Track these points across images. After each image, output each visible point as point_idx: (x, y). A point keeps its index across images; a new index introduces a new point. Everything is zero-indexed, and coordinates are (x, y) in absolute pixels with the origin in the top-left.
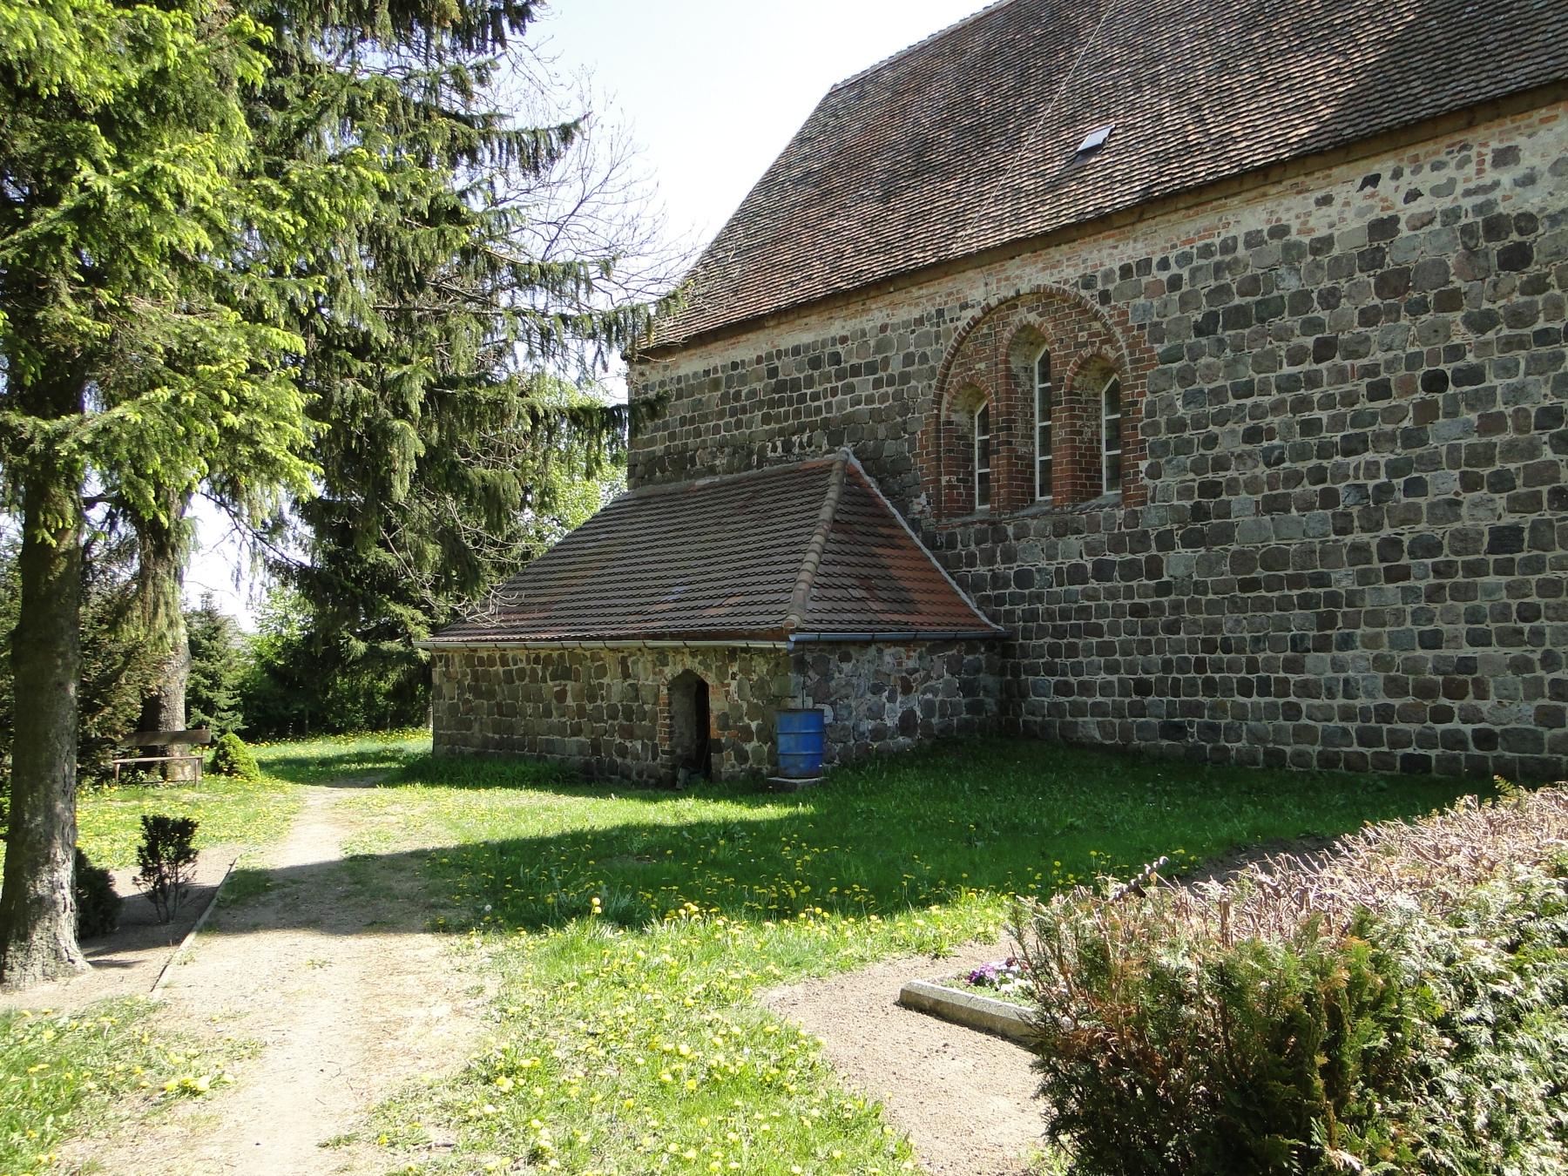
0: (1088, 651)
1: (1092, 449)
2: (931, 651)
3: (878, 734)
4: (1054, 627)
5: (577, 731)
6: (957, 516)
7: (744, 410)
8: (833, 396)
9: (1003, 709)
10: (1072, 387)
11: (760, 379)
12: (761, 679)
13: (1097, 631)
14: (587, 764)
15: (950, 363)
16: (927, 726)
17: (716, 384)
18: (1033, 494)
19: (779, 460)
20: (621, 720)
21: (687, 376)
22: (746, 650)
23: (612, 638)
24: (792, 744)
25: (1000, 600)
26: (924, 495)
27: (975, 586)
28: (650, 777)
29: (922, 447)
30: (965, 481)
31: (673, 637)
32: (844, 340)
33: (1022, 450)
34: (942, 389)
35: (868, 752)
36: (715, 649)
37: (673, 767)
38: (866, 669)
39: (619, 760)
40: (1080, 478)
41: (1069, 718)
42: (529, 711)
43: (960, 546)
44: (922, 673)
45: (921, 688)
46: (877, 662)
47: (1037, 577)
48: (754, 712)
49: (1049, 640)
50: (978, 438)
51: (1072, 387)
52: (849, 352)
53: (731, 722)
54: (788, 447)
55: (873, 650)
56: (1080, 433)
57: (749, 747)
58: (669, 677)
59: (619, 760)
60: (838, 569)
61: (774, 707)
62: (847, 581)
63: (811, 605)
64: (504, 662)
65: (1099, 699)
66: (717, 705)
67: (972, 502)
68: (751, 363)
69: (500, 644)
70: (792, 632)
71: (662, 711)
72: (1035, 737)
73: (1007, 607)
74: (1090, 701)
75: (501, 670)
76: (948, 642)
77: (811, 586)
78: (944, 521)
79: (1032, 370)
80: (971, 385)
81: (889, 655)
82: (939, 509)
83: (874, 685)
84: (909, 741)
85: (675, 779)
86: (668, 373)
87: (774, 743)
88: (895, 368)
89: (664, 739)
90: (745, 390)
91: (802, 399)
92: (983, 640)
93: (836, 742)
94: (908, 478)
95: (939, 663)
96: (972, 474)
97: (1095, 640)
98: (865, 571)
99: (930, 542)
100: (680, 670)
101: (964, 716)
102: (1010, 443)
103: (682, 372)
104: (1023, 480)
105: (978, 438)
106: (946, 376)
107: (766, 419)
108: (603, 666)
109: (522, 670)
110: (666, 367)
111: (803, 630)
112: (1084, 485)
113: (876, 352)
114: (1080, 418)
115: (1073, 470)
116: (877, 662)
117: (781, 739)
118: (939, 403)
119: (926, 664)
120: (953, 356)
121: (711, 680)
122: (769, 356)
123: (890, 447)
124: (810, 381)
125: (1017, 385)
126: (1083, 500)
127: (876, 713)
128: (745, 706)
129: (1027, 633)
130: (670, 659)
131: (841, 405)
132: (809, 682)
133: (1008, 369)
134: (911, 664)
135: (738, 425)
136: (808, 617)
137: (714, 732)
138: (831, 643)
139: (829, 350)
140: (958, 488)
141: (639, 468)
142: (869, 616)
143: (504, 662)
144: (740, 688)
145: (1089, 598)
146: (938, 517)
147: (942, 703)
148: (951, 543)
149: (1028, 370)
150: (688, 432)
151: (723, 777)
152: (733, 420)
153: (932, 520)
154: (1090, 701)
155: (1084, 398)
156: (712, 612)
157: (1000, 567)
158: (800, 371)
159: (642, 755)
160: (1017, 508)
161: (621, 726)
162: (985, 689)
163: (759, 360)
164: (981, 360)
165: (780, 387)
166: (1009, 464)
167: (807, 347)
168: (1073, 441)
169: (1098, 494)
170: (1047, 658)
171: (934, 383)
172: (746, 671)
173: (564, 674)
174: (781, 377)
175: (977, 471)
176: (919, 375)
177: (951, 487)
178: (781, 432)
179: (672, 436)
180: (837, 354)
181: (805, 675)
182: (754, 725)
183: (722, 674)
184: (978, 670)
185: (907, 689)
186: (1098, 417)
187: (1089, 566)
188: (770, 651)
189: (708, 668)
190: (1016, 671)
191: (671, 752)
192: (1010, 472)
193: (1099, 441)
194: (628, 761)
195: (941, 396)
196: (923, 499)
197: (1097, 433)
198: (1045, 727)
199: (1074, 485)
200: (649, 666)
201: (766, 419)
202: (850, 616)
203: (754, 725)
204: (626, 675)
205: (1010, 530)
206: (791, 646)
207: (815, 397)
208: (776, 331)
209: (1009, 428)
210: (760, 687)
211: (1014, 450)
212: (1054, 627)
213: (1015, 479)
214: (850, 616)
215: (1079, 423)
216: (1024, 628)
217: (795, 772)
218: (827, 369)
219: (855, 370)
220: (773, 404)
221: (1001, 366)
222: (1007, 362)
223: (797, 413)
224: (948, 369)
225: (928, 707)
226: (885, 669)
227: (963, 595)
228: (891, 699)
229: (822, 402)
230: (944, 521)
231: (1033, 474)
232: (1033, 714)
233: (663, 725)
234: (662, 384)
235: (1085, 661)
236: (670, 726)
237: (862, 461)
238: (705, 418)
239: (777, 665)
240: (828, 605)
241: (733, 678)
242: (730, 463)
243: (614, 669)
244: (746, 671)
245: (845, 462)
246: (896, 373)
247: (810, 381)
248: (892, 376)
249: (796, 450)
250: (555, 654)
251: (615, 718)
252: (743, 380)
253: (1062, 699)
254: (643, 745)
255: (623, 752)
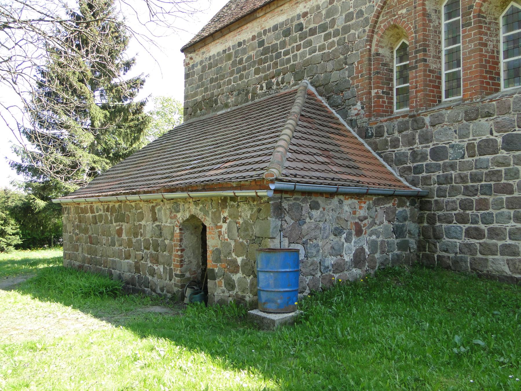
0: (499, 205)
1: (493, 57)
2: (377, 203)
3: (338, 268)
4: (466, 188)
5: (128, 257)
6: (382, 116)
7: (244, 69)
8: (298, 50)
9: (421, 247)
10: (480, 11)
11: (253, 49)
12: (245, 222)
13: (508, 189)
14: (133, 278)
15: (380, 13)
16: (373, 260)
17: (229, 57)
18: (440, 97)
19: (265, 94)
20: (151, 251)
21: (214, 55)
22: (234, 199)
23: (145, 192)
24: (271, 281)
25: (418, 170)
26: (359, 104)
27: (399, 161)
28: (168, 292)
29: (359, 72)
30: (388, 94)
31: (183, 190)
32: (305, 15)
33: (433, 66)
34: (373, 32)
35: (331, 281)
36: (211, 198)
37: (183, 286)
38: (330, 216)
39: (150, 278)
40: (485, 78)
41: (479, 256)
42: (104, 242)
43: (386, 134)
44: (370, 220)
45: (368, 231)
46: (338, 210)
47: (451, 151)
48: (240, 249)
49: (461, 197)
50: (396, 65)
51: (480, 11)
52: (309, 22)
53: (222, 256)
54: (269, 87)
55: (335, 200)
56: (486, 45)
57: (236, 277)
58: (181, 221)
59: (150, 278)
60: (306, 143)
61: (256, 246)
62: (314, 151)
63: (288, 164)
64: (92, 212)
65: (509, 242)
66: (212, 242)
67: (391, 108)
68: (249, 41)
69: (88, 199)
70: (272, 181)
71: (175, 245)
72: (448, 268)
73: (424, 174)
74: (500, 243)
75: (91, 215)
76: (389, 197)
77: (287, 151)
78: (373, 119)
79: (440, 12)
80: (395, 26)
81: (348, 204)
82: (370, 112)
83: (336, 229)
84: (359, 271)
85: (183, 297)
86: (204, 56)
87: (255, 276)
88: (340, 24)
89: (176, 266)
90: (245, 57)
91: (278, 56)
92: (408, 196)
93: (306, 275)
94: (347, 94)
95: (380, 212)
96: (391, 89)
97: (504, 197)
98: (325, 146)
99: (365, 134)
100: (187, 215)
101: (396, 252)
102: (425, 60)
103: (211, 54)
104: (434, 87)
105: (396, 65)
106: (376, 22)
107: (257, 72)
108: (141, 213)
109: (101, 216)
110: (203, 53)
111: (281, 180)
112: (488, 83)
113: (325, 18)
114: (486, 34)
115: (482, 72)
116: (338, 210)
117: (261, 276)
118: (371, 41)
119: (372, 212)
120: (382, 8)
121: (208, 223)
122: (260, 35)
123: (335, 76)
124: (283, 44)
125: (430, 21)
126: (488, 94)
127: (337, 251)
128: (233, 244)
129: (441, 193)
130: (181, 207)
131: (303, 55)
132: (285, 226)
133: (424, 9)
134: (362, 213)
135: (241, 77)
136: (284, 172)
137: (210, 264)
138: (304, 193)
139: (296, 22)
140: (382, 97)
141: (189, 109)
142: (332, 175)
143: (92, 212)
144: (229, 229)
145: (499, 164)
146: (369, 116)
147: (382, 242)
148: (380, 134)
149: (437, 12)
150: (214, 86)
151: (216, 299)
152: (238, 75)
153: (365, 119)
154: (500, 243)
155: (487, 20)
156: (212, 173)
157: (418, 146)
158: (277, 39)
159: (163, 276)
160: (430, 106)
161: (151, 254)
162: (410, 233)
163: (254, 38)
164: (402, 8)
165: (266, 51)
166: (425, 75)
167: (282, 24)
168: (481, 50)
169: (497, 90)
170: (459, 211)
171: (367, 28)
172: (235, 216)
173: (121, 219)
174: (266, 45)
175: (395, 87)
176: (356, 26)
177: (378, 97)
178: (265, 78)
179: (206, 90)
180: (301, 24)
181: (282, 219)
182: (239, 260)
183: (216, 218)
184: (405, 219)
185: (359, 232)
186: (497, 35)
187: (500, 140)
188: (253, 199)
189: (206, 213)
190: (432, 220)
191: (182, 276)
192: (425, 80)
193: (498, 52)
194: (155, 279)
195: (372, 37)
196: (359, 106)
197: (497, 46)
198: (456, 262)
199: (482, 82)
200: (168, 212)
201: (257, 72)
202: (318, 174)
203: (239, 260)
204: (155, 219)
205: (427, 120)
206: (271, 194)
207: (287, 53)
208: (263, 19)
209: (425, 50)
210: (243, 229)
211: (427, 66)
212: (466, 188)
213: (429, 86)
214: (318, 174)
215: (485, 38)
216: (439, 189)
217: (271, 306)
218: (294, 34)
219: (313, 32)
220: (261, 62)
221: (419, 8)
222: (423, 4)
223: (276, 64)
224: (378, 17)
225: (373, 245)
226: (344, 216)
227: (389, 168)
228: (348, 240)
229: (291, 56)
230: (373, 119)
231: (440, 83)
232: (446, 251)
233: (176, 256)
234: (202, 62)
235: (495, 212)
236: (182, 256)
237: (316, 87)
238: (223, 77)
239: (259, 210)
240: (301, 165)
241: (224, 222)
242: (236, 100)
243: (148, 215)
244: (235, 216)
245: (306, 87)
246: (340, 28)
247: (283, 44)
248: (338, 30)
249: (275, 87)
250: (117, 205)
251: (148, 249)
252: (244, 51)
253: (473, 241)
254: (164, 268)
255: (153, 273)
